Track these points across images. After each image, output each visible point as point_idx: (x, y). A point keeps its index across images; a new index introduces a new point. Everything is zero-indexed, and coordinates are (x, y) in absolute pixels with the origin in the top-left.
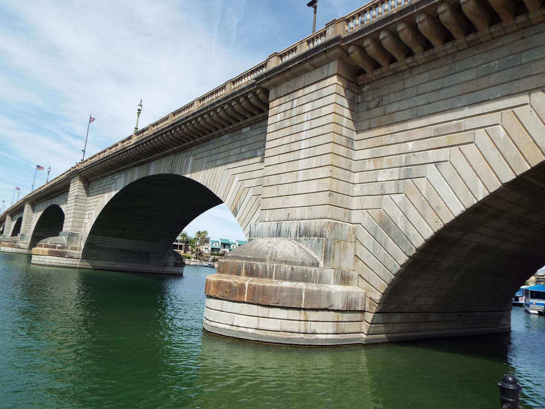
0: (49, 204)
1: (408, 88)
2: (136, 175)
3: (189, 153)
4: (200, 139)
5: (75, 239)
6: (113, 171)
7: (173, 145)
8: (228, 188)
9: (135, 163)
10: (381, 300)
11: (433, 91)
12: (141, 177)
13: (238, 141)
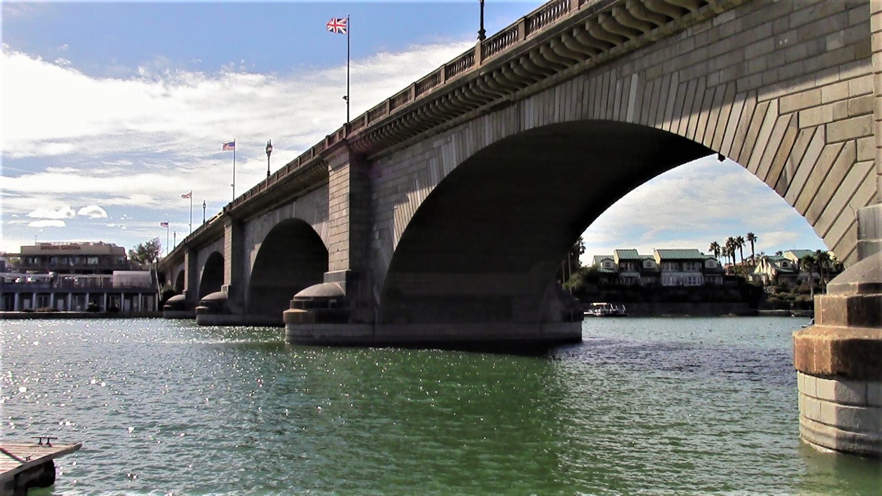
0: (278, 217)
3: (627, 68)
6: (427, 132)
9: (484, 107)
12: (503, 136)
13: (763, 23)
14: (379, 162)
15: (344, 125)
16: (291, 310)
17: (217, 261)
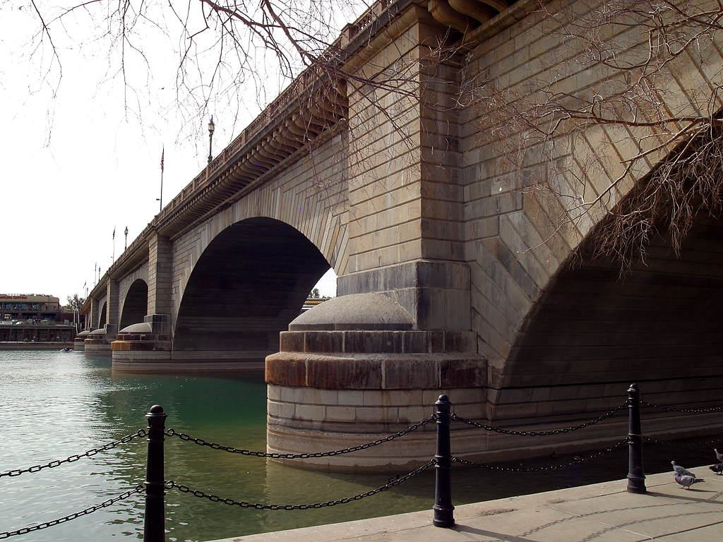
1: (519, 50)
2: (220, 224)
4: (284, 161)
5: (162, 325)
6: (194, 222)
7: (260, 171)
8: (323, 228)
9: (217, 207)
10: (505, 368)
11: (549, 51)
14: (176, 242)
15: (344, 30)
16: (281, 355)
17: (139, 289)
